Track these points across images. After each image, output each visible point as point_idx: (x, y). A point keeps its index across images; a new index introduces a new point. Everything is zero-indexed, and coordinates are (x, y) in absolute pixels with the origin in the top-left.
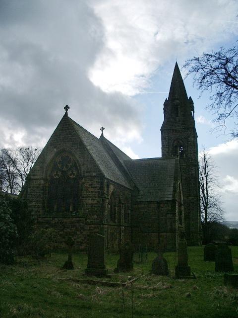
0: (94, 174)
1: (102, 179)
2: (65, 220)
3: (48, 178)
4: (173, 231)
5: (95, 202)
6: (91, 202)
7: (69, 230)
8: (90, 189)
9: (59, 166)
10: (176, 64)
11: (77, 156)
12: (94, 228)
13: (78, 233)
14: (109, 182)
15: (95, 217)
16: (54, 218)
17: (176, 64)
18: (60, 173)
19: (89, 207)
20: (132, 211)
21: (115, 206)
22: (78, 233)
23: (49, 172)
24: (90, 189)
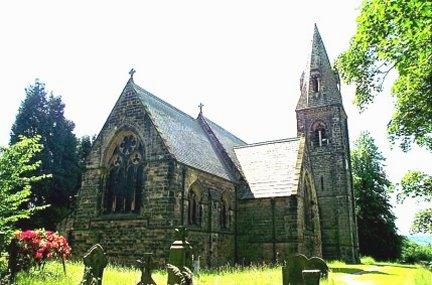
0: (161, 157)
1: (171, 164)
2: (123, 224)
3: (107, 165)
4: (293, 239)
5: (161, 196)
6: (156, 196)
7: (126, 237)
8: (156, 179)
9: (121, 149)
10: (318, 40)
11: (141, 134)
12: (159, 233)
13: (138, 241)
14: (185, 169)
15: (161, 217)
16: (109, 221)
17: (318, 40)
18: (121, 159)
19: (153, 203)
20: (236, 211)
21: (200, 203)
22: (138, 241)
23: (109, 156)
24: (156, 179)
